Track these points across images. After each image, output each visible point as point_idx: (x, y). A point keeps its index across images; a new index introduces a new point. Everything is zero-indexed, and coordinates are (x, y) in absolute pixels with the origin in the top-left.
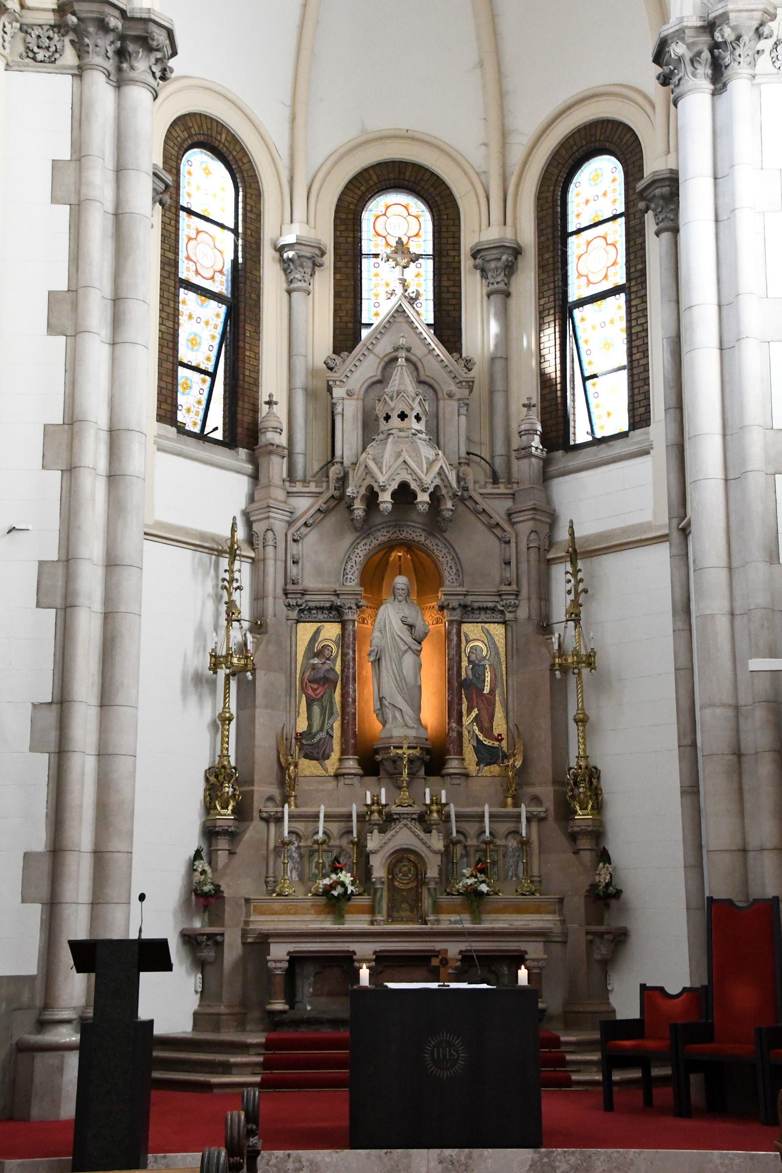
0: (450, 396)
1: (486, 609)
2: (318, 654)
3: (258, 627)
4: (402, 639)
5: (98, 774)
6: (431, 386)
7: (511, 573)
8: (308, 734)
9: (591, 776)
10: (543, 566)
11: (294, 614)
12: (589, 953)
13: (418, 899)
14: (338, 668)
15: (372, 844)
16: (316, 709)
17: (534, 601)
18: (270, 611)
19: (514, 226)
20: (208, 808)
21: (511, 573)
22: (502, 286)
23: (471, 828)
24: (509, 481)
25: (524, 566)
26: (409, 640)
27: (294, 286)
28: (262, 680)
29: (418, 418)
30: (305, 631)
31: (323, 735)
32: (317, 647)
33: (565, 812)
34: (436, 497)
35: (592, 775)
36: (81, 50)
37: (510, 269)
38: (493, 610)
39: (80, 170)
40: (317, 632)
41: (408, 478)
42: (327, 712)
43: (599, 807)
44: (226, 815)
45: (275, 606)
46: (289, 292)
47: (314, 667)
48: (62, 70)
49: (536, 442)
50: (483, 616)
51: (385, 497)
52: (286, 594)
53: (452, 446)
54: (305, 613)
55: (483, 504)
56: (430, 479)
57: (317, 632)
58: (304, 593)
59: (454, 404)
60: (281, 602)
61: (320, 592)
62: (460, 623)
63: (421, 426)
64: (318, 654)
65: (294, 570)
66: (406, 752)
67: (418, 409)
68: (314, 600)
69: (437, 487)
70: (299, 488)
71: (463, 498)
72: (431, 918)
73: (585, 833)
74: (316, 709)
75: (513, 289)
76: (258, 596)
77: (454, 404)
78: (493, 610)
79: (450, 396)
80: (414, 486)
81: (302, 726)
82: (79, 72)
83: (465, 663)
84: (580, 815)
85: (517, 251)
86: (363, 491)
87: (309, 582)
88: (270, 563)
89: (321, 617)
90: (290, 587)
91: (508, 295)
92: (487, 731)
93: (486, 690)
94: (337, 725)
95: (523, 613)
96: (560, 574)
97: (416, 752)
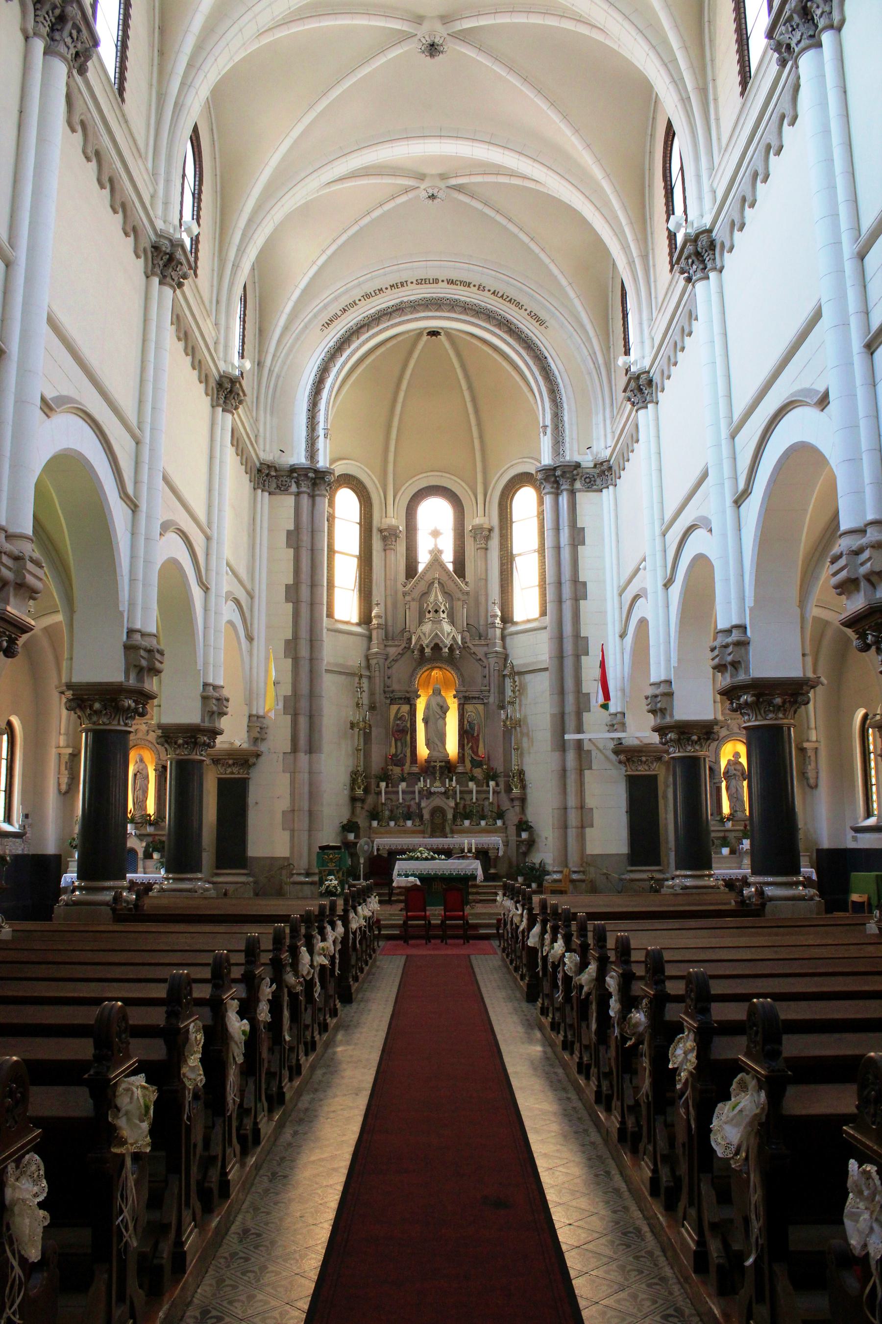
0: (459, 599)
1: (474, 698)
2: (400, 719)
3: (372, 708)
4: (341, 179)
5: (194, 640)
6: (449, 594)
7: (486, 681)
8: (395, 755)
9: (520, 774)
10: (501, 679)
11: (388, 701)
12: (517, 851)
13: (444, 828)
14: (409, 725)
15: (423, 804)
16: (399, 744)
17: (496, 694)
18: (378, 700)
19: (489, 517)
20: (352, 789)
21: (486, 681)
22: (483, 546)
23: (467, 797)
24: (486, 639)
25: (492, 678)
26: (441, 713)
27: (387, 547)
28: (375, 732)
29: (443, 612)
30: (394, 708)
31: (402, 755)
32: (399, 715)
33: (509, 790)
34: (451, 649)
35: (521, 773)
36: (298, 485)
37: (488, 538)
38: (478, 698)
39: (298, 533)
40: (399, 709)
41: (438, 642)
42: (404, 744)
43: (524, 787)
44: (359, 792)
45: (379, 697)
46: (385, 550)
47: (398, 725)
48: (291, 494)
49: (498, 621)
50: (474, 701)
51: (427, 650)
52: (385, 692)
53: (459, 622)
54: (393, 701)
55: (473, 649)
56: (448, 642)
57: (399, 709)
58: (393, 692)
59: (460, 603)
60: (382, 697)
61: (400, 691)
62: (464, 704)
63: (445, 616)
64: (400, 719)
65: (388, 682)
66: (438, 764)
67: (443, 608)
68: (398, 695)
69: (452, 645)
70: (390, 643)
71: (465, 647)
72: (449, 835)
73: (517, 799)
74: (399, 744)
75: (489, 546)
76: (372, 694)
77: (460, 603)
78: (478, 698)
79: (459, 599)
80: (441, 645)
81: (393, 751)
82: (298, 494)
83: (466, 722)
84: (515, 791)
85: (490, 530)
86: (418, 647)
87: (395, 686)
88: (377, 679)
89: (401, 702)
90: (386, 689)
91: (487, 549)
92: (476, 753)
93: (475, 734)
94: (408, 751)
95: (491, 700)
96: (508, 682)
97: (443, 764)
